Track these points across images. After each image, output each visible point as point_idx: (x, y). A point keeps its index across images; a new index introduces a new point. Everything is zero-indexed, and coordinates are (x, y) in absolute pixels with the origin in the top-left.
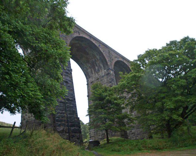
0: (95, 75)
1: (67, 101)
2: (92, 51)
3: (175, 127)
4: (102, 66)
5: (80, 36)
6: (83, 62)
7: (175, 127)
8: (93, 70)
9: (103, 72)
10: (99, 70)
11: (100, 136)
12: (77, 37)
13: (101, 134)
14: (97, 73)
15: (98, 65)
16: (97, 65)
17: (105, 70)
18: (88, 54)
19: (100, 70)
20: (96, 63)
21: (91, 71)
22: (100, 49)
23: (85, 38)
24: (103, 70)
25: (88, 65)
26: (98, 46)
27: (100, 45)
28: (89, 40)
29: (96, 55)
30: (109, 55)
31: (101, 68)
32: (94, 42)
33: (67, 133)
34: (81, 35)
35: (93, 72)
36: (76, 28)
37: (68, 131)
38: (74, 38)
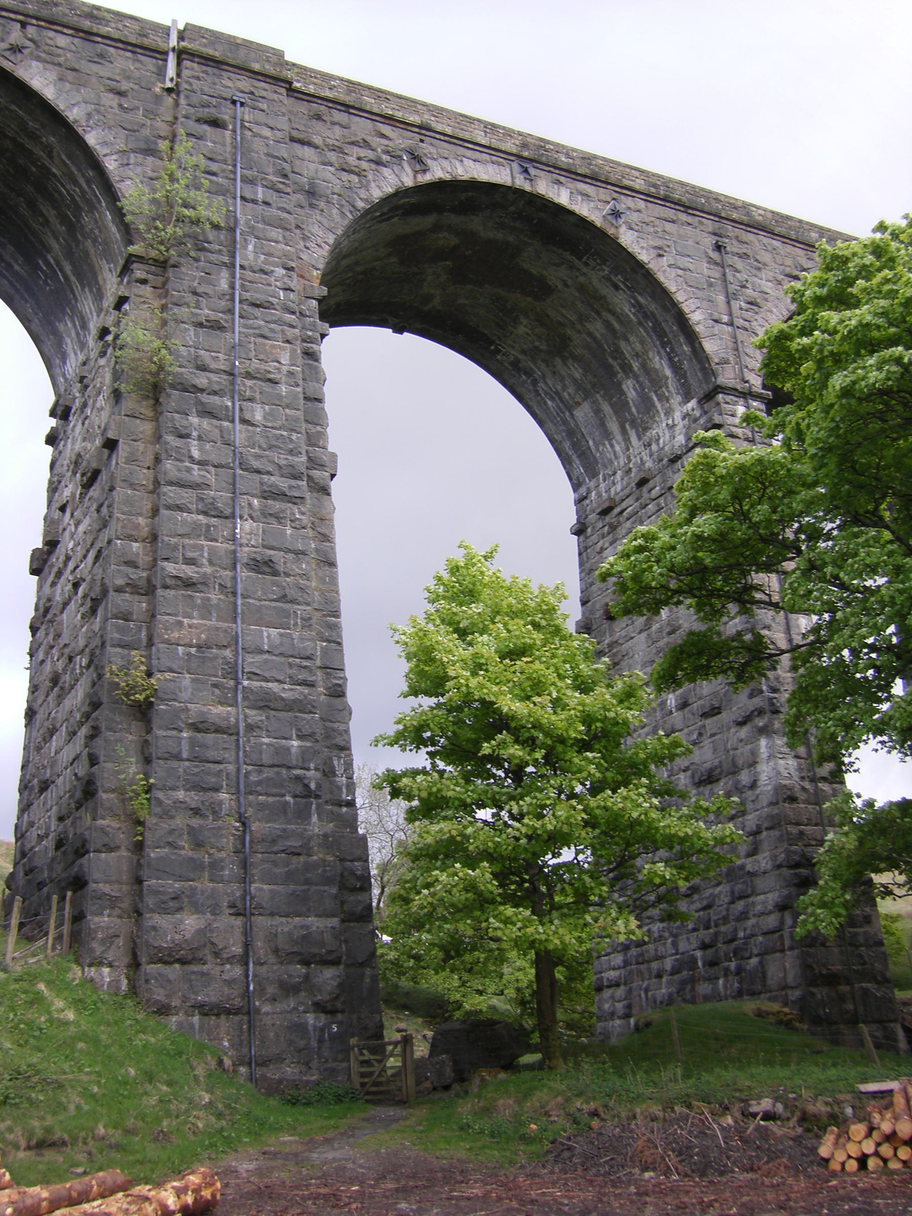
0: (627, 440)
1: (255, 716)
2: (572, 267)
3: (305, 1104)
4: (668, 372)
5: (427, 178)
6: (523, 352)
7: (305, 1104)
8: (606, 408)
9: (677, 415)
10: (647, 407)
11: (659, 976)
12: (401, 193)
13: (668, 964)
14: (642, 428)
15: (636, 365)
16: (627, 368)
17: (692, 404)
18: (543, 289)
19: (658, 405)
20: (618, 353)
21: (598, 411)
22: (627, 238)
23: (473, 185)
24: (676, 400)
25: (563, 371)
26: (598, 222)
27: (625, 203)
28: (520, 193)
29: (606, 291)
30: (716, 273)
31: (657, 382)
32: (563, 197)
33: (229, 960)
34: (438, 172)
35: (613, 426)
36: (386, 130)
37: (237, 949)
38: (367, 212)
